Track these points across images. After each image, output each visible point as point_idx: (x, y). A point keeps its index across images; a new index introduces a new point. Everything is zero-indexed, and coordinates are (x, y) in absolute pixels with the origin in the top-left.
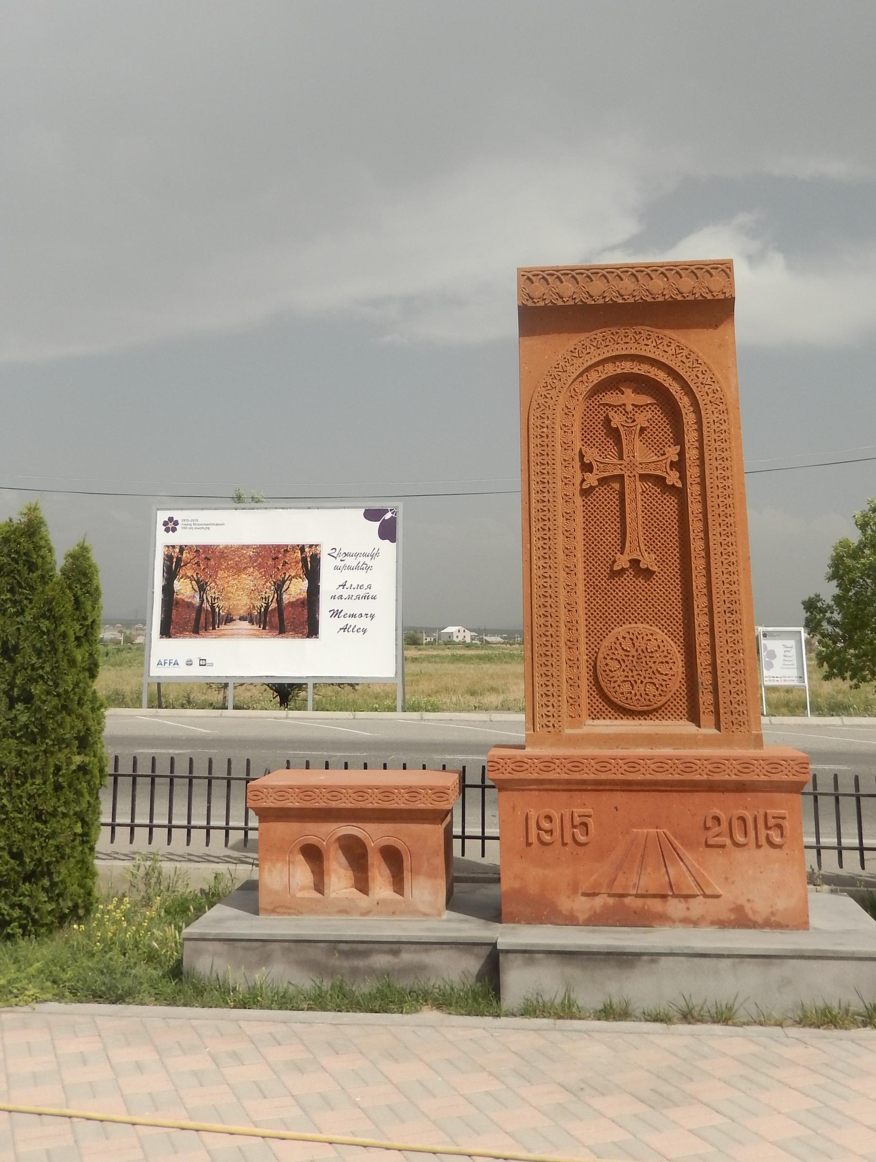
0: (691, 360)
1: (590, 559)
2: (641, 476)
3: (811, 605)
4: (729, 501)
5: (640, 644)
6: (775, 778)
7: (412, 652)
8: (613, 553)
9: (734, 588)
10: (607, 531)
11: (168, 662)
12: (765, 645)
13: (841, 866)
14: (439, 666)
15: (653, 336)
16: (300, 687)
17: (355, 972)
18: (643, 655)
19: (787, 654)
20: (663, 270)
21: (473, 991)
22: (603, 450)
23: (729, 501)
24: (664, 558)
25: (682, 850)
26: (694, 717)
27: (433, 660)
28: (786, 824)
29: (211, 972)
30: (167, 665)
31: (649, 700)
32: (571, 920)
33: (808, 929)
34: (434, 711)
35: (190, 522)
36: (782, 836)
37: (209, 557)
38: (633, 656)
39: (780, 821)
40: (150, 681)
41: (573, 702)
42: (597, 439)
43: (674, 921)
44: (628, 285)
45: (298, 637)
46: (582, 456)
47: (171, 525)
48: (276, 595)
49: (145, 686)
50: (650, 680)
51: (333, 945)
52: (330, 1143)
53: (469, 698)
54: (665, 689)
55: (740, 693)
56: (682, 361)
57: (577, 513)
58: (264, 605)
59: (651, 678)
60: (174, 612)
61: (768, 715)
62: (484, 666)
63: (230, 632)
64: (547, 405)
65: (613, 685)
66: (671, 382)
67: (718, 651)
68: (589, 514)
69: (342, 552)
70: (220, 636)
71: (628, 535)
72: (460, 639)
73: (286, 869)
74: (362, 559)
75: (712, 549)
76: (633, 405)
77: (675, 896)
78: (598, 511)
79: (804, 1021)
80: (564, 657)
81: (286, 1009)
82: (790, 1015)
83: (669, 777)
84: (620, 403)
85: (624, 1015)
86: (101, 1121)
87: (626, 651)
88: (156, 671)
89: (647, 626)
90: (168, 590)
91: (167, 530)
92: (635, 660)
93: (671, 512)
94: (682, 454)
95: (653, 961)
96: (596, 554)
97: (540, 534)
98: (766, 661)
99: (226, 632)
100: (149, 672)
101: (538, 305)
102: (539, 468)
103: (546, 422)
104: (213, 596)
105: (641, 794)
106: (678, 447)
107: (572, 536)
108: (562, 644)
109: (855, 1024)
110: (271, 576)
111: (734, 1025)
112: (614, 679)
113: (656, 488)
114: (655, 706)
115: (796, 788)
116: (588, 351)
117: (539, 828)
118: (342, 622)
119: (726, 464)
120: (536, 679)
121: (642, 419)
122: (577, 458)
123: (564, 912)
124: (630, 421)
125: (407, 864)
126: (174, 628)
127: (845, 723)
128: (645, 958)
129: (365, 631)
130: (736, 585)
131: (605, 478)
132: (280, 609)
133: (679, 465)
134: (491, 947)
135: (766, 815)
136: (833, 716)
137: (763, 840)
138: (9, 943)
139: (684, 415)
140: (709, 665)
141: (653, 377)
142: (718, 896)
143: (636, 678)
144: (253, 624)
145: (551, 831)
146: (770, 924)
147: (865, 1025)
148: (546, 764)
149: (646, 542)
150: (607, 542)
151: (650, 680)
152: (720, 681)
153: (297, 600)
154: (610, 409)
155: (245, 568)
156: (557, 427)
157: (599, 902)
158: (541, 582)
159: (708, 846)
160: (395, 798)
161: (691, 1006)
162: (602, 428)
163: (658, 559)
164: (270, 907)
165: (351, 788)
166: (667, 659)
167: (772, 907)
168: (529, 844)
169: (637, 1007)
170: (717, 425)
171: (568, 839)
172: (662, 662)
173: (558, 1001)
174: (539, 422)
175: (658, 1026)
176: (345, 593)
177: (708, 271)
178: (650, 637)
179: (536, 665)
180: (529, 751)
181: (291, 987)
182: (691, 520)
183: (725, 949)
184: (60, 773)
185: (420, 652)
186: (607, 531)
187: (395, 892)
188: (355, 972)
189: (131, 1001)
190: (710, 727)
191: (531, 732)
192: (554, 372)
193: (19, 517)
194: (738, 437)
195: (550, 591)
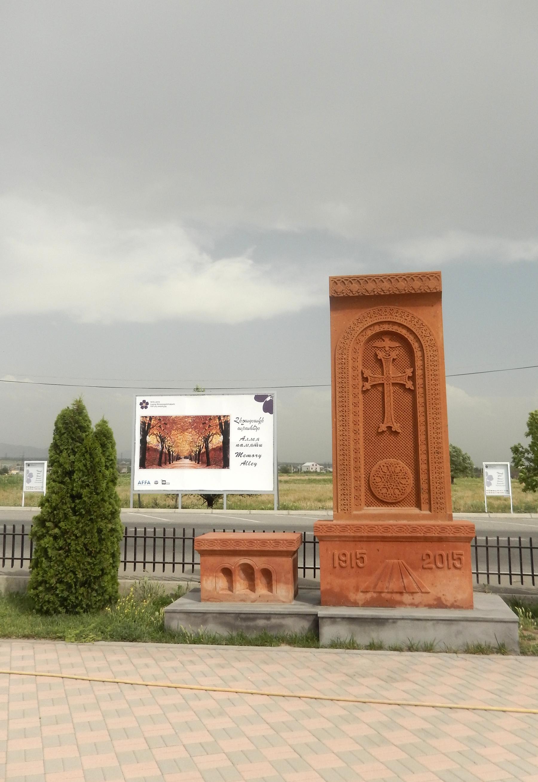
0: (419, 324)
1: (367, 426)
2: (392, 383)
3: (516, 450)
4: (437, 397)
5: (392, 469)
6: (458, 535)
7: (285, 478)
8: (378, 423)
9: (440, 441)
10: (375, 412)
11: (144, 482)
12: (487, 473)
13: (500, 583)
14: (300, 485)
15: (400, 311)
16: (219, 496)
17: (248, 628)
18: (393, 475)
19: (500, 477)
20: (404, 277)
21: (306, 637)
22: (373, 370)
23: (437, 397)
24: (404, 426)
25: (411, 570)
26: (418, 505)
27: (298, 482)
28: (463, 558)
29: (178, 627)
30: (144, 484)
31: (396, 497)
32: (355, 604)
33: (473, 609)
34: (296, 510)
35: (155, 403)
36: (461, 563)
37: (166, 422)
38: (388, 475)
39: (460, 556)
40: (134, 493)
41: (357, 498)
42: (370, 365)
43: (406, 605)
44: (386, 285)
45: (218, 468)
46: (362, 374)
47: (144, 405)
48: (205, 444)
49: (132, 496)
50: (396, 487)
51: (238, 615)
52: (236, 693)
53: (316, 503)
54: (403, 491)
55: (441, 493)
56: (414, 325)
57: (360, 403)
58: (198, 450)
59: (397, 486)
60: (147, 454)
61: (488, 512)
62: (327, 485)
63: (179, 465)
64: (344, 347)
65: (377, 489)
66: (408, 335)
67: (431, 472)
68: (366, 403)
69: (242, 419)
70: (173, 468)
71: (386, 414)
72: (314, 470)
73: (214, 580)
74: (254, 424)
75: (428, 421)
76: (389, 347)
77: (407, 593)
78: (371, 402)
79: (468, 651)
80: (353, 476)
81: (215, 644)
82: (461, 648)
83: (405, 535)
84: (383, 346)
85: (380, 647)
86: (132, 684)
87: (384, 472)
88: (137, 487)
89: (395, 460)
90: (143, 442)
91: (142, 408)
92: (389, 477)
93: (408, 402)
94: (414, 372)
95: (394, 622)
96: (370, 424)
97: (341, 414)
98: (487, 482)
99: (176, 465)
100: (134, 488)
101: (340, 296)
102: (340, 380)
103: (344, 356)
104: (169, 445)
105: (391, 543)
106: (412, 369)
107: (357, 415)
108: (352, 469)
109: (493, 653)
110: (202, 433)
111: (434, 652)
112: (378, 486)
113: (400, 390)
114: (399, 500)
115: (468, 540)
116: (366, 319)
117: (340, 559)
118: (243, 459)
119: (437, 377)
120: (339, 487)
121: (394, 355)
122: (360, 375)
123: (352, 601)
124: (387, 355)
125: (274, 577)
126: (147, 463)
127: (533, 517)
128: (391, 621)
129: (255, 465)
130: (440, 439)
131: (375, 385)
132: (207, 452)
133: (412, 378)
134: (315, 616)
135: (453, 553)
136: (526, 513)
137: (451, 566)
138: (78, 616)
139: (415, 353)
140: (426, 479)
141: (400, 333)
142: (428, 593)
143: (389, 486)
144: (192, 461)
145: (346, 561)
146: (454, 606)
147: (497, 653)
148: (343, 528)
149: (395, 417)
150: (375, 418)
151: (396, 487)
152: (431, 487)
153: (217, 447)
154: (377, 349)
155: (187, 429)
156: (350, 359)
157: (369, 596)
158: (341, 438)
159: (423, 568)
160: (268, 545)
161: (413, 643)
162: (373, 359)
163: (401, 426)
164: (207, 598)
165: (246, 540)
166: (405, 477)
167: (455, 598)
168: (335, 567)
169: (386, 644)
170: (432, 357)
171: (354, 565)
172: (403, 478)
173: (348, 641)
174: (340, 356)
175: (396, 652)
176: (244, 443)
177: (428, 278)
178: (397, 465)
179: (338, 479)
180: (335, 522)
181: (217, 635)
182: (418, 406)
183: (429, 617)
184: (103, 533)
185: (290, 478)
186: (375, 412)
187: (268, 591)
188: (248, 628)
189: (140, 641)
190: (426, 511)
191: (336, 513)
192: (348, 331)
193: (72, 406)
194: (443, 363)
195: (346, 443)
